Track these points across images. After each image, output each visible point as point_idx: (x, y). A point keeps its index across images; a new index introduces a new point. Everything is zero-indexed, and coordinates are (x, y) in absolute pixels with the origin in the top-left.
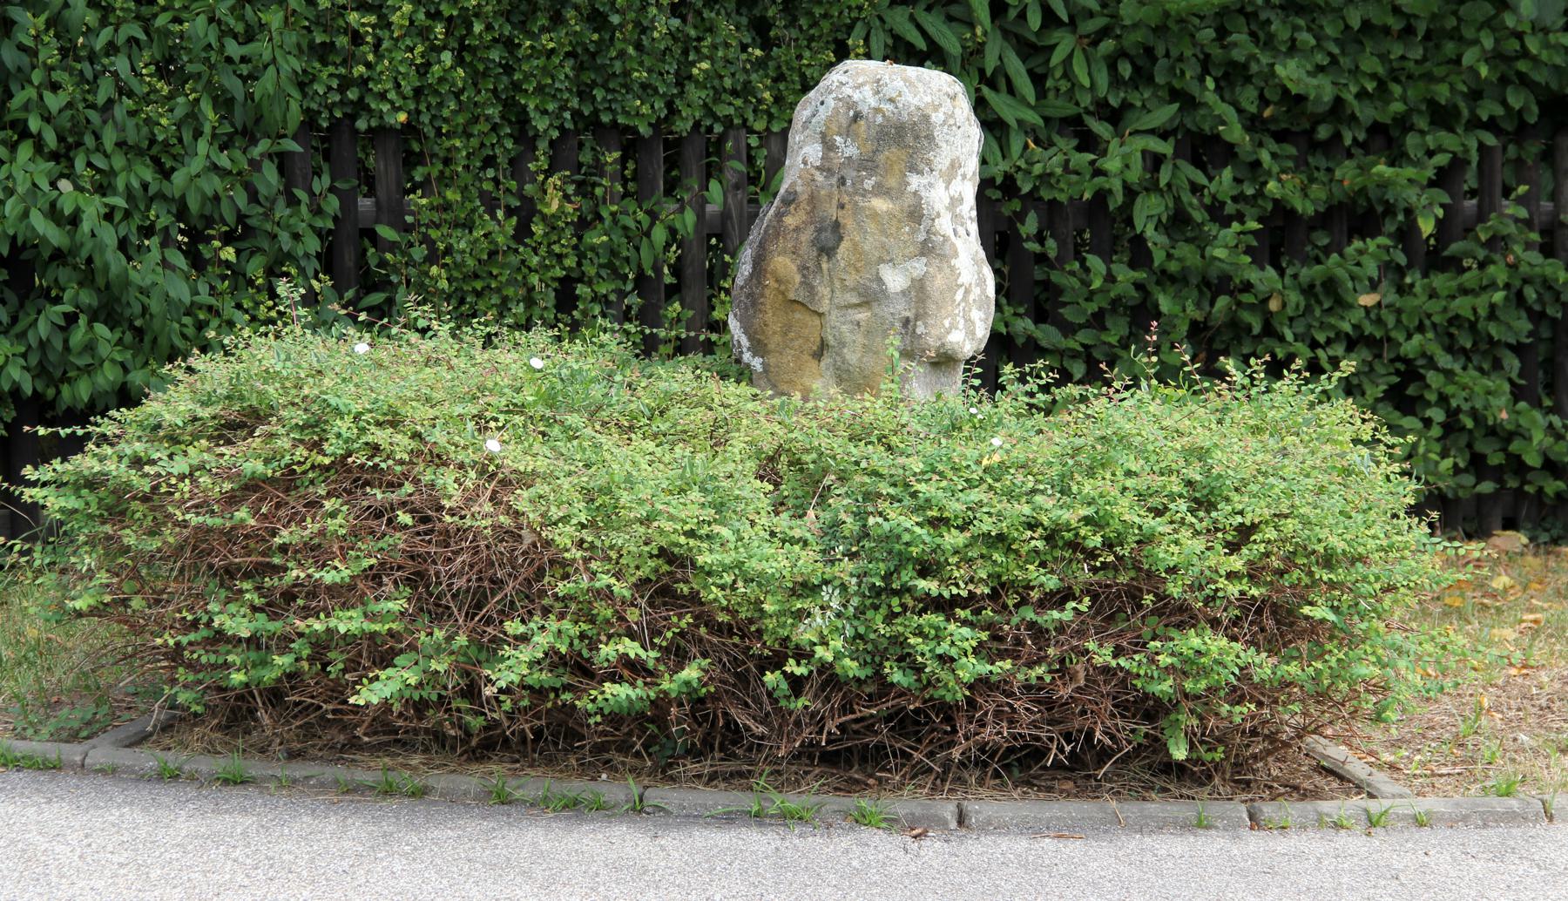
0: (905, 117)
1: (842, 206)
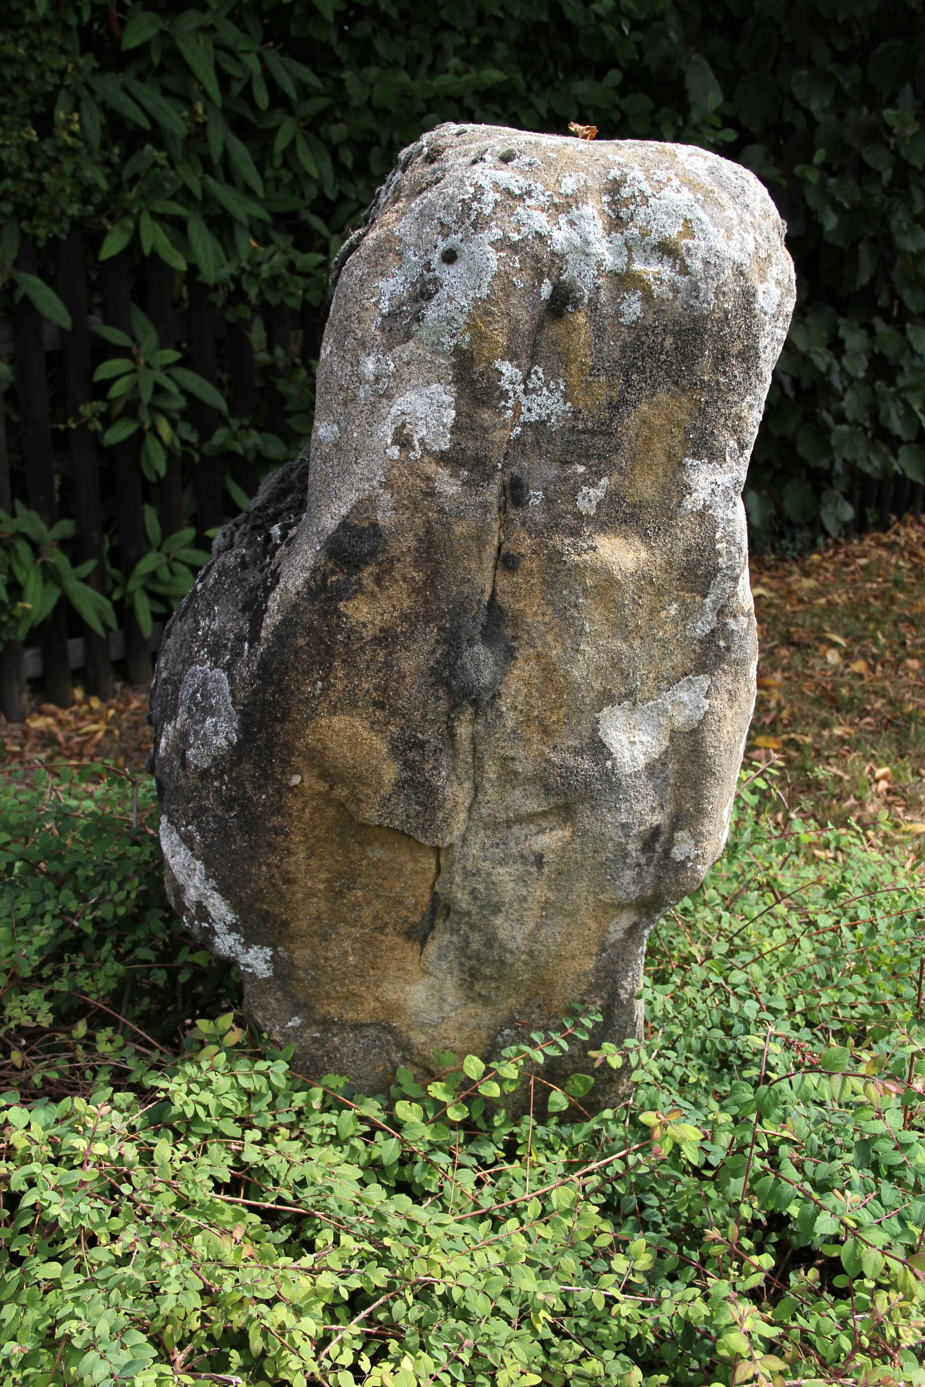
0: (709, 302)
1: (507, 562)
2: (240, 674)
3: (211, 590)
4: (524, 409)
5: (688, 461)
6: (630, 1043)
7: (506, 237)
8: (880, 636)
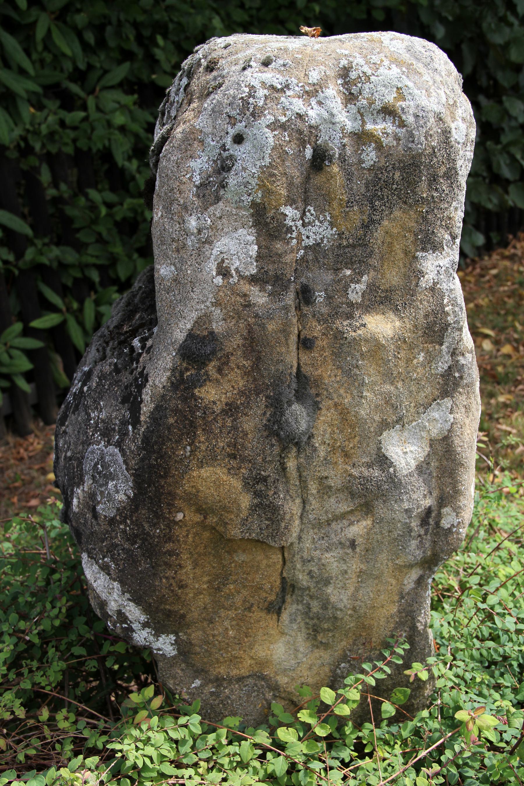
0: (422, 144)
1: (306, 344)
2: (130, 448)
3: (95, 391)
4: (304, 237)
5: (419, 254)
6: (431, 660)
7: (277, 120)
8: (517, 325)
